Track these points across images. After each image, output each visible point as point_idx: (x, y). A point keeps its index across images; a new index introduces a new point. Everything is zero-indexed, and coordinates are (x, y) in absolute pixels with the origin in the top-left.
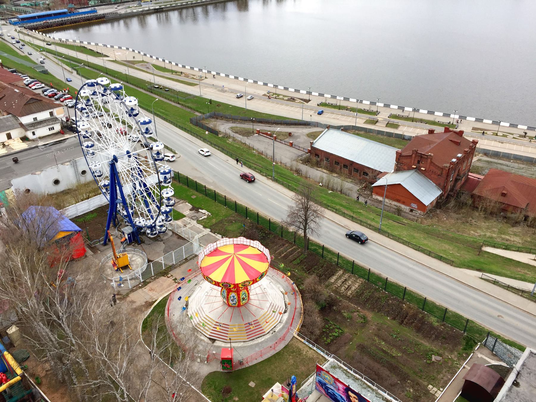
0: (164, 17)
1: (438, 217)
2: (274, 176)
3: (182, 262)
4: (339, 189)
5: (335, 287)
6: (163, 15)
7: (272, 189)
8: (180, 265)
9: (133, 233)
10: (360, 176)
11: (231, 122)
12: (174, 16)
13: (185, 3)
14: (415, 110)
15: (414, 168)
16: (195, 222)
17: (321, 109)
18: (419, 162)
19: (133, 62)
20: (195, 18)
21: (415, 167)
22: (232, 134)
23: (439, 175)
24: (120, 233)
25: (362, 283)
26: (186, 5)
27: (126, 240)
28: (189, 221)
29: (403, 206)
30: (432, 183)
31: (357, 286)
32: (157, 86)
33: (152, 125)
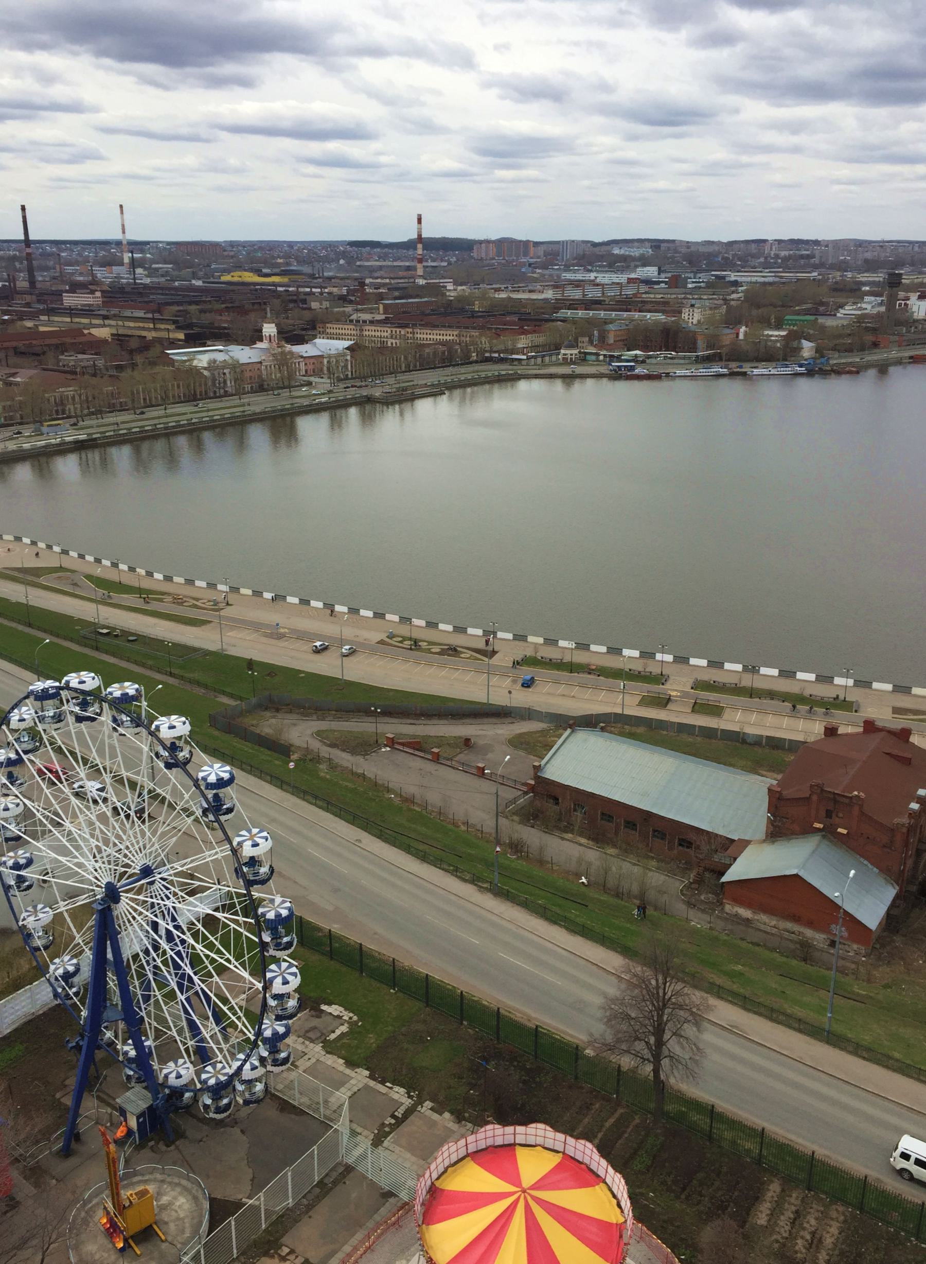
0: (97, 458)
1: (902, 958)
2: (496, 881)
3: (311, 1197)
4: (635, 889)
5: (777, 1241)
6: (94, 456)
7: (489, 916)
8: (310, 1207)
9: (150, 1108)
10: (671, 849)
11: (315, 717)
12: (122, 456)
13: (150, 428)
14: (751, 669)
15: (819, 830)
16: (318, 1048)
17: (527, 672)
18: (829, 814)
19: (37, 572)
20: (172, 460)
21: (821, 826)
22: (325, 751)
23: (884, 846)
24: (109, 1110)
25: (845, 1221)
26: (152, 430)
27: (130, 1132)
28: (300, 1048)
29: (809, 933)
30: (869, 865)
31: (834, 1229)
32: (105, 631)
33: (232, 789)
